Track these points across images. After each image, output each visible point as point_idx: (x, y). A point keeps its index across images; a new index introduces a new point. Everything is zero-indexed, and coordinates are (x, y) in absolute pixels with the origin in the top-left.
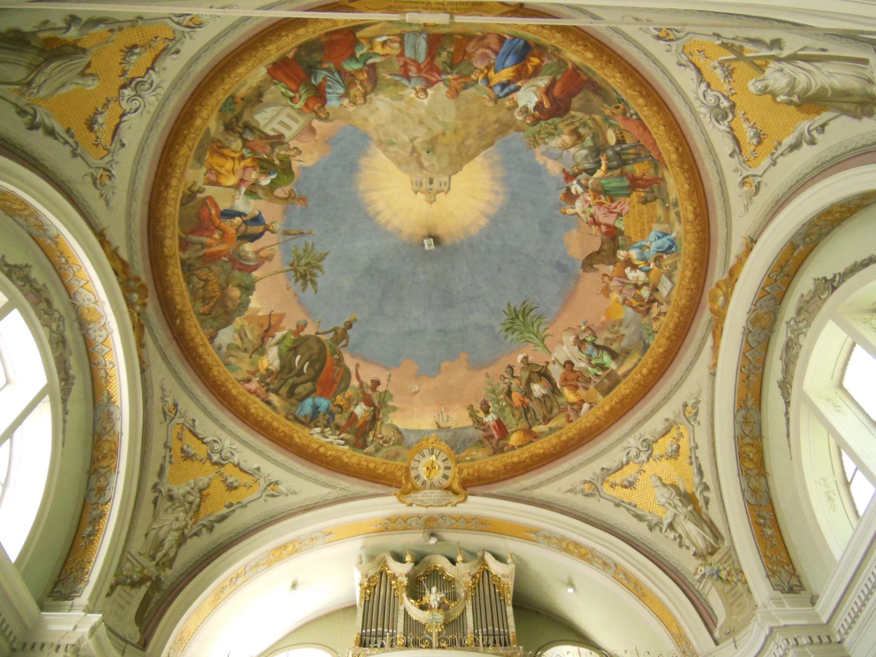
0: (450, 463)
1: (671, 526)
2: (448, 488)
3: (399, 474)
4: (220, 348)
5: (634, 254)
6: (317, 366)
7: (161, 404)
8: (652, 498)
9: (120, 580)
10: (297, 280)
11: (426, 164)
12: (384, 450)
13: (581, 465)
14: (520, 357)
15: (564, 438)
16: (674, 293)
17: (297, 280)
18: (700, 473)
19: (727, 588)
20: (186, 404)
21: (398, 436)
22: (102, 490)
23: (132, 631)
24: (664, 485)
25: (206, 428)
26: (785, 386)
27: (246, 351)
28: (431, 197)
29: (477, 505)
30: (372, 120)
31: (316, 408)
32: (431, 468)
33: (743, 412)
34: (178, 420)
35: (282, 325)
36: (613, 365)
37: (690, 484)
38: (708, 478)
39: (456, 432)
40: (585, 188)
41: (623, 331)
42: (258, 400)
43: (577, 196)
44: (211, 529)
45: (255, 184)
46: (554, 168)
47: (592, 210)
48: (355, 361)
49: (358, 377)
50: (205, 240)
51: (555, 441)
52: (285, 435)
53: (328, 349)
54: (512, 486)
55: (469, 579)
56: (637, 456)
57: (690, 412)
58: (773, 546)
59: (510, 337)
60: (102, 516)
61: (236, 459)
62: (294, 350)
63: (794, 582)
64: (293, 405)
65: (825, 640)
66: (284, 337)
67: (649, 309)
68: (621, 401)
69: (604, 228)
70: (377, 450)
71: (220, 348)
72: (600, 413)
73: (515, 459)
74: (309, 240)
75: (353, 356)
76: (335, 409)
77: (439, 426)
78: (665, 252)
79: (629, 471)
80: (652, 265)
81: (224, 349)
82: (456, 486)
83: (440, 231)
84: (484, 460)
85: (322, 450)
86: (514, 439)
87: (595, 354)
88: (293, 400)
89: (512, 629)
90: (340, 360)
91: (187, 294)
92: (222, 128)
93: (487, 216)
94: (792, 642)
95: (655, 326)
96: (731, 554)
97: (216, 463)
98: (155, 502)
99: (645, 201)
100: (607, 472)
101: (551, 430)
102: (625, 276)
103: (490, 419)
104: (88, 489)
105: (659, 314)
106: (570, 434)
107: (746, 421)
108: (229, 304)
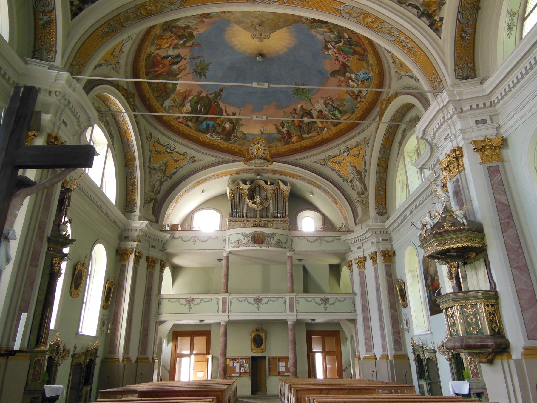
0: (266, 148)
1: (351, 181)
2: (264, 159)
3: (245, 152)
4: (165, 108)
5: (353, 76)
6: (208, 108)
7: (145, 135)
8: (347, 170)
9: (146, 202)
10: (197, 75)
11: (258, 29)
12: (238, 142)
13: (321, 152)
14: (299, 106)
15: (315, 141)
16: (368, 95)
17: (197, 75)
18: (365, 165)
19: (365, 207)
20: (155, 133)
21: (244, 136)
22: (132, 173)
23: (152, 218)
24: (352, 166)
25: (164, 140)
26: (400, 143)
27: (176, 107)
28: (261, 40)
29: (276, 166)
30: (232, 17)
31: (208, 125)
32: (258, 149)
33: (384, 149)
34: (152, 140)
35: (191, 94)
36: (339, 116)
37: (361, 168)
38: (367, 168)
39: (270, 135)
40: (334, 47)
41: (345, 103)
42: (183, 125)
43: (330, 49)
44: (171, 178)
45: (177, 44)
46: (320, 37)
47: (337, 55)
48: (224, 105)
49: (226, 112)
50: (157, 69)
51: (311, 142)
52: (196, 137)
53: (212, 101)
54: (291, 158)
55: (272, 191)
56: (344, 153)
57: (366, 141)
58: (381, 198)
59: (296, 97)
60: (134, 182)
61: (177, 150)
62: (197, 103)
63: (384, 211)
64: (198, 125)
65: (385, 233)
66: (192, 99)
67: (357, 98)
68: (341, 130)
69: (341, 63)
70: (235, 142)
71: (165, 108)
72: (331, 133)
73: (294, 147)
74: (202, 59)
75: (224, 103)
76: (216, 125)
77: (262, 133)
78: (366, 80)
79: (340, 158)
80: (360, 83)
81: (167, 108)
82: (268, 157)
83: (265, 52)
84: (281, 147)
85: (211, 142)
86: (294, 139)
87: (332, 109)
88: (198, 123)
89: (287, 211)
90: (218, 105)
91: (150, 91)
92: (162, 31)
93: (288, 48)
94: (374, 233)
95: (358, 105)
96: (367, 197)
97: (169, 153)
98: (150, 172)
99: (359, 60)
100: (331, 157)
101: (310, 137)
102: (348, 83)
103: (284, 130)
104: (127, 173)
105: (361, 101)
106: (318, 140)
107: (384, 152)
108: (168, 90)
